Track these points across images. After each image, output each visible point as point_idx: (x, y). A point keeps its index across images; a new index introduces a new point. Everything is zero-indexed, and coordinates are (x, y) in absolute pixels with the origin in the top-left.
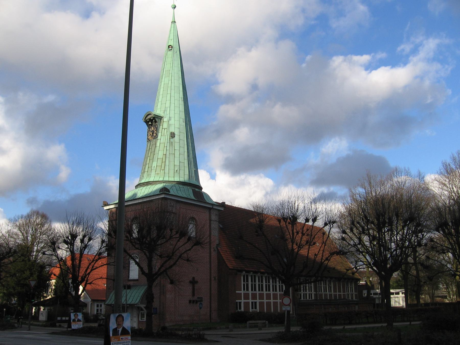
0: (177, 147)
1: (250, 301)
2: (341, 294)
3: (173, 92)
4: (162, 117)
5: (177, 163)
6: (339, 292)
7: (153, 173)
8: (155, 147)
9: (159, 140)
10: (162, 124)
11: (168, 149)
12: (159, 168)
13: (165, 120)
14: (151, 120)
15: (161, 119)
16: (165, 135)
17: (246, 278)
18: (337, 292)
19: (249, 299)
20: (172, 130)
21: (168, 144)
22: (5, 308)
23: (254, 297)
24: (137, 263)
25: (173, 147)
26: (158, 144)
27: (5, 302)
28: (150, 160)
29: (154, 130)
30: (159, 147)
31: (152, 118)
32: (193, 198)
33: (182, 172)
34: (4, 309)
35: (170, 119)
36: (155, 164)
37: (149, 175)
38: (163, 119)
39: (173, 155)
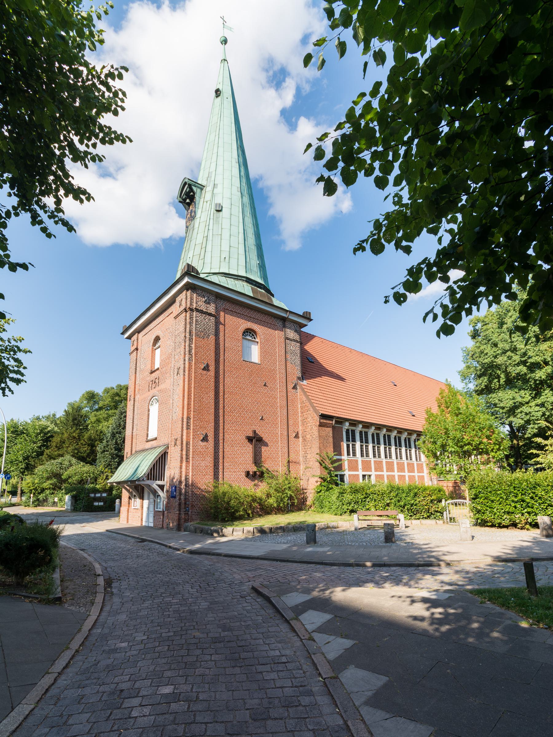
0: (226, 224)
1: (361, 473)
2: (394, 476)
3: (221, 150)
4: (204, 186)
5: (225, 247)
6: (409, 471)
9: (198, 219)
10: (203, 196)
11: (211, 227)
13: (209, 189)
15: (202, 189)
16: (207, 209)
17: (352, 436)
18: (383, 471)
19: (358, 470)
20: (218, 200)
21: (211, 220)
22: (480, 98)
23: (367, 466)
24: (498, 267)
25: (220, 225)
26: (196, 226)
27: (65, 69)
32: (252, 295)
33: (234, 262)
34: (507, 85)
35: (215, 186)
38: (205, 189)
39: (220, 236)
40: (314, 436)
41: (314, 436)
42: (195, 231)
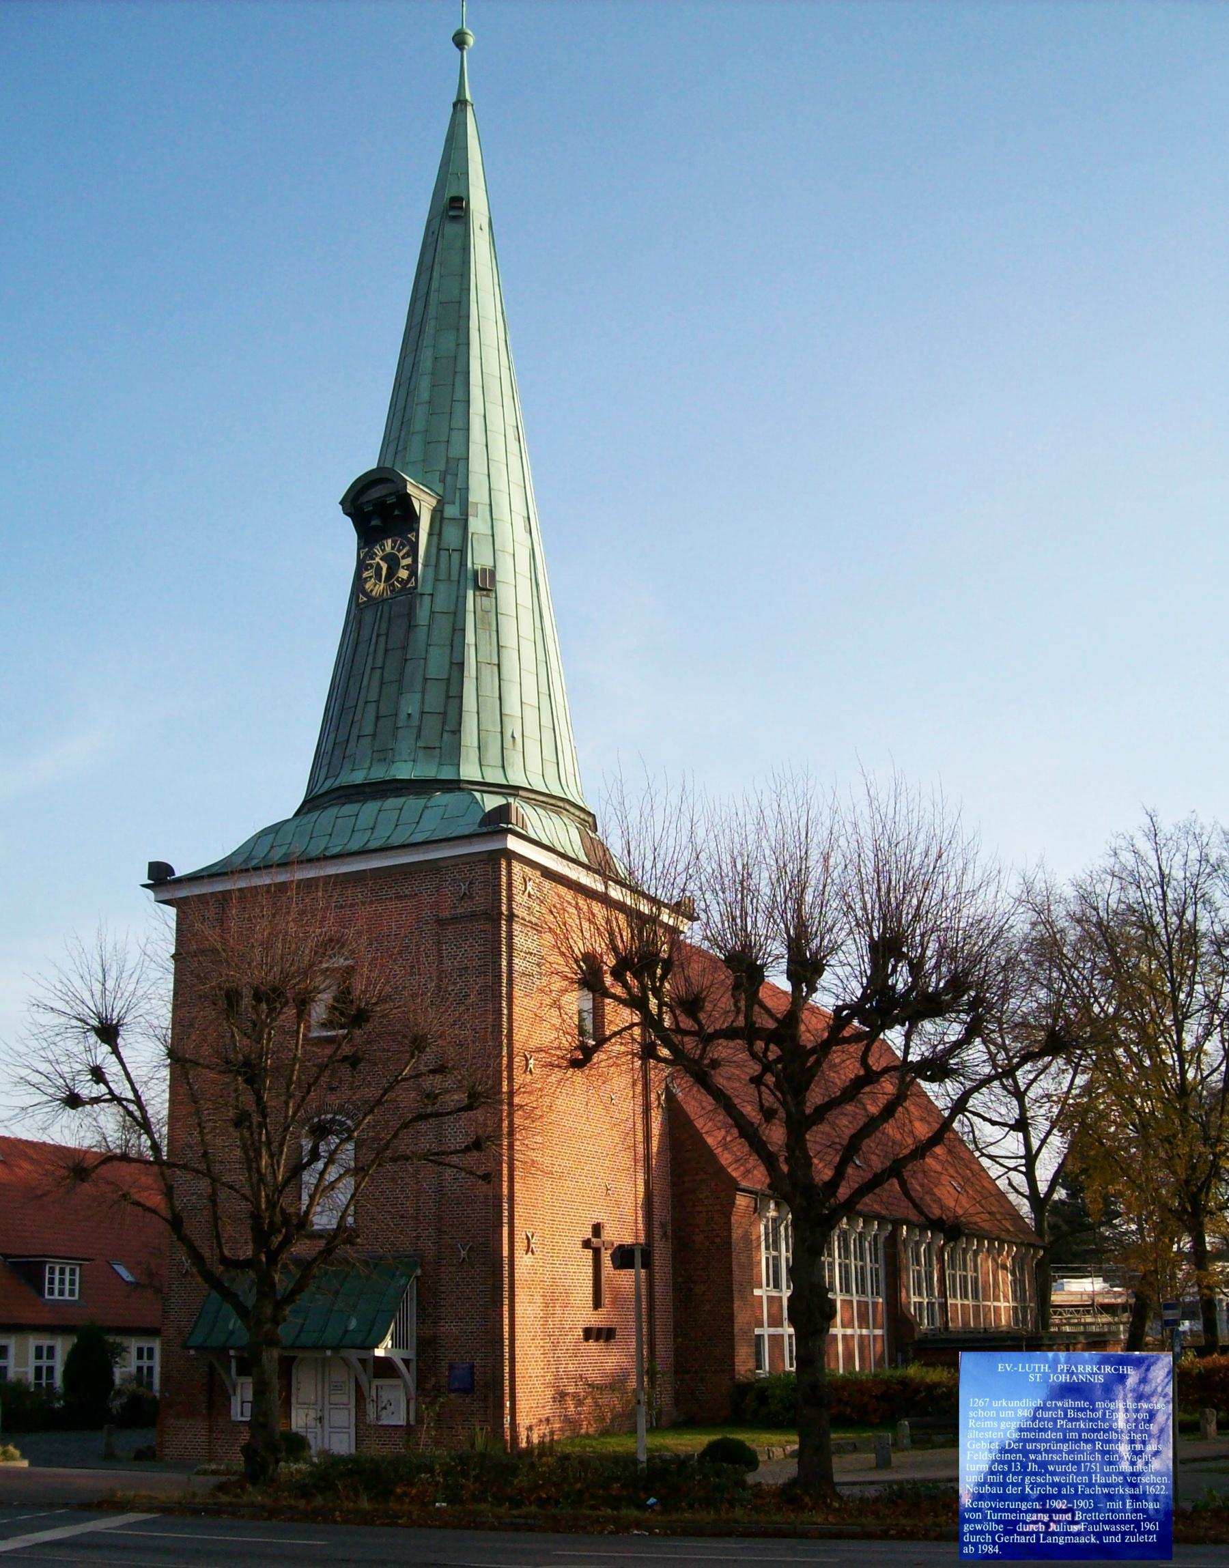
7: (405, 744)
8: (410, 627)
12: (431, 724)
14: (381, 507)
28: (386, 651)
29: (400, 555)
30: (426, 628)
31: (391, 500)
36: (410, 705)
37: (384, 755)
40: (717, 1240)
41: (717, 1240)
42: (421, 633)
